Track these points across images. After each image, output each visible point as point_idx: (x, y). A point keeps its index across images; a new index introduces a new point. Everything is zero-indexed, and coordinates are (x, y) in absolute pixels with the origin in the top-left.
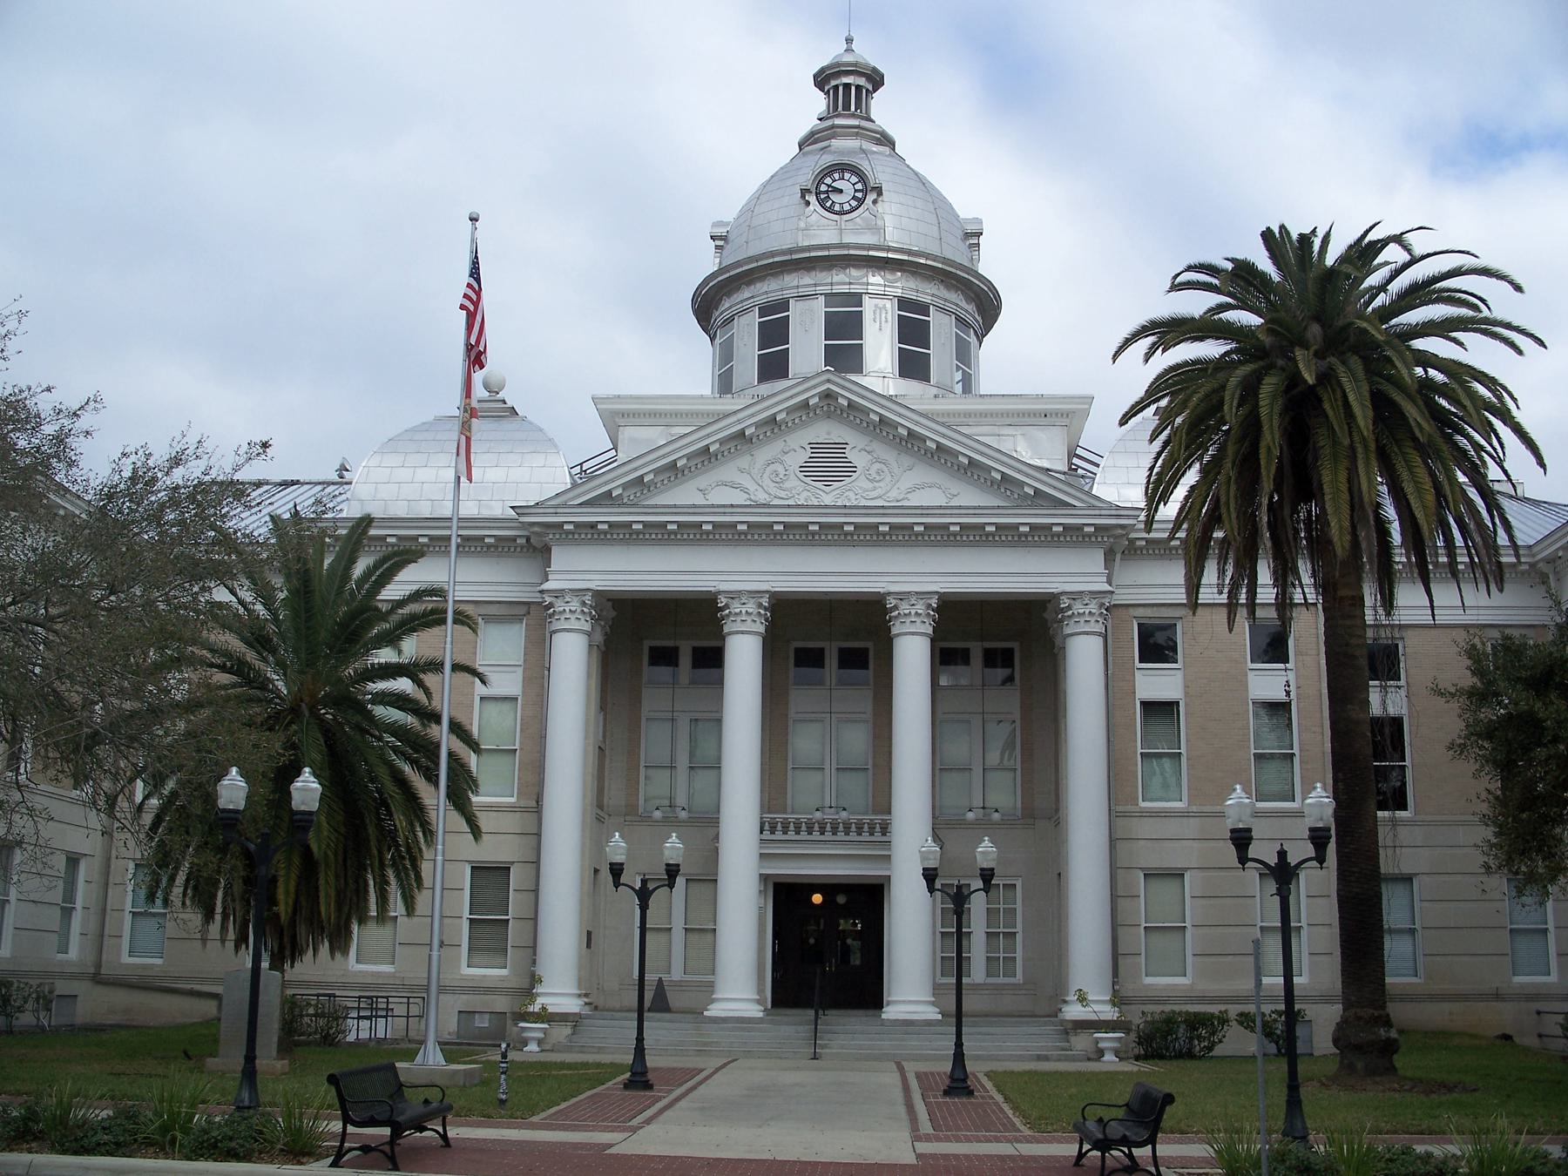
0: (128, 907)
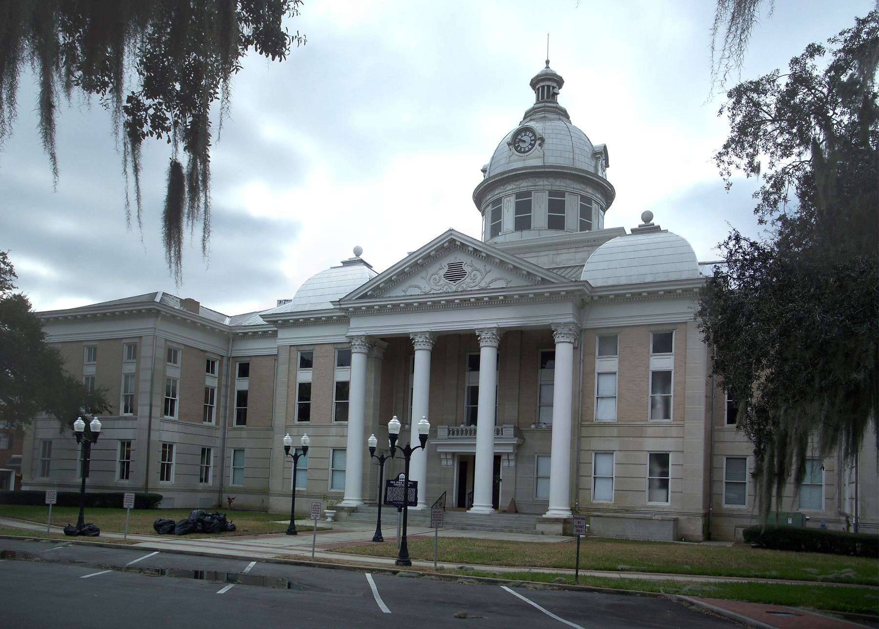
0: (232, 466)
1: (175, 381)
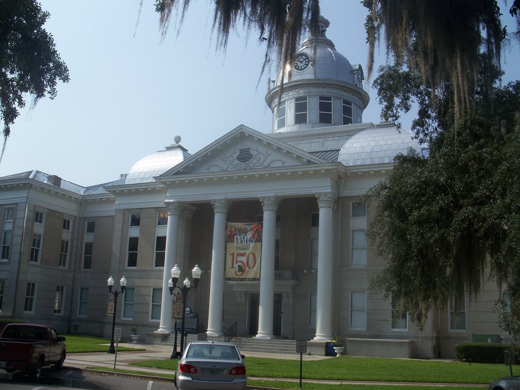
0: (79, 301)
1: (40, 236)
